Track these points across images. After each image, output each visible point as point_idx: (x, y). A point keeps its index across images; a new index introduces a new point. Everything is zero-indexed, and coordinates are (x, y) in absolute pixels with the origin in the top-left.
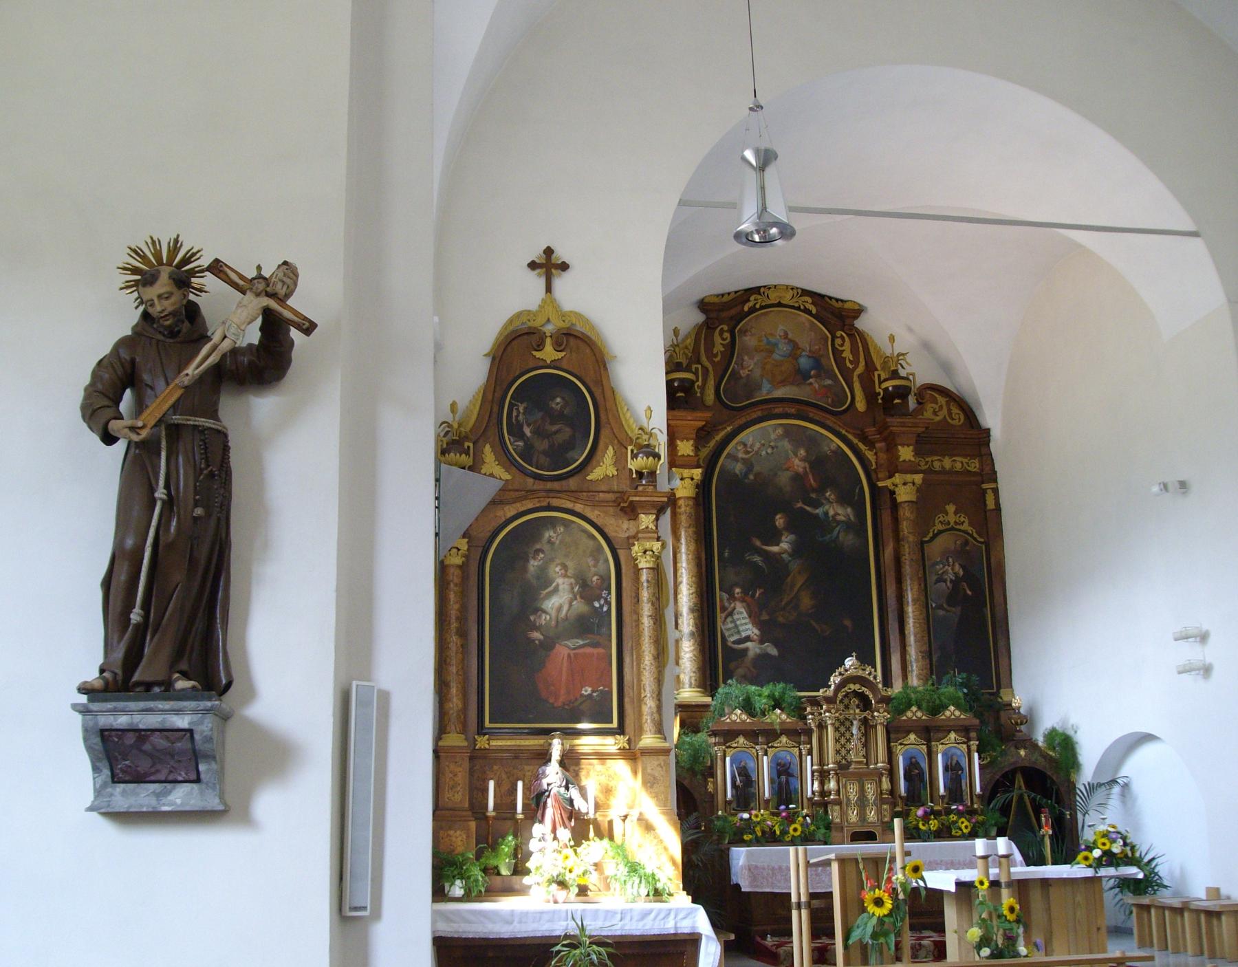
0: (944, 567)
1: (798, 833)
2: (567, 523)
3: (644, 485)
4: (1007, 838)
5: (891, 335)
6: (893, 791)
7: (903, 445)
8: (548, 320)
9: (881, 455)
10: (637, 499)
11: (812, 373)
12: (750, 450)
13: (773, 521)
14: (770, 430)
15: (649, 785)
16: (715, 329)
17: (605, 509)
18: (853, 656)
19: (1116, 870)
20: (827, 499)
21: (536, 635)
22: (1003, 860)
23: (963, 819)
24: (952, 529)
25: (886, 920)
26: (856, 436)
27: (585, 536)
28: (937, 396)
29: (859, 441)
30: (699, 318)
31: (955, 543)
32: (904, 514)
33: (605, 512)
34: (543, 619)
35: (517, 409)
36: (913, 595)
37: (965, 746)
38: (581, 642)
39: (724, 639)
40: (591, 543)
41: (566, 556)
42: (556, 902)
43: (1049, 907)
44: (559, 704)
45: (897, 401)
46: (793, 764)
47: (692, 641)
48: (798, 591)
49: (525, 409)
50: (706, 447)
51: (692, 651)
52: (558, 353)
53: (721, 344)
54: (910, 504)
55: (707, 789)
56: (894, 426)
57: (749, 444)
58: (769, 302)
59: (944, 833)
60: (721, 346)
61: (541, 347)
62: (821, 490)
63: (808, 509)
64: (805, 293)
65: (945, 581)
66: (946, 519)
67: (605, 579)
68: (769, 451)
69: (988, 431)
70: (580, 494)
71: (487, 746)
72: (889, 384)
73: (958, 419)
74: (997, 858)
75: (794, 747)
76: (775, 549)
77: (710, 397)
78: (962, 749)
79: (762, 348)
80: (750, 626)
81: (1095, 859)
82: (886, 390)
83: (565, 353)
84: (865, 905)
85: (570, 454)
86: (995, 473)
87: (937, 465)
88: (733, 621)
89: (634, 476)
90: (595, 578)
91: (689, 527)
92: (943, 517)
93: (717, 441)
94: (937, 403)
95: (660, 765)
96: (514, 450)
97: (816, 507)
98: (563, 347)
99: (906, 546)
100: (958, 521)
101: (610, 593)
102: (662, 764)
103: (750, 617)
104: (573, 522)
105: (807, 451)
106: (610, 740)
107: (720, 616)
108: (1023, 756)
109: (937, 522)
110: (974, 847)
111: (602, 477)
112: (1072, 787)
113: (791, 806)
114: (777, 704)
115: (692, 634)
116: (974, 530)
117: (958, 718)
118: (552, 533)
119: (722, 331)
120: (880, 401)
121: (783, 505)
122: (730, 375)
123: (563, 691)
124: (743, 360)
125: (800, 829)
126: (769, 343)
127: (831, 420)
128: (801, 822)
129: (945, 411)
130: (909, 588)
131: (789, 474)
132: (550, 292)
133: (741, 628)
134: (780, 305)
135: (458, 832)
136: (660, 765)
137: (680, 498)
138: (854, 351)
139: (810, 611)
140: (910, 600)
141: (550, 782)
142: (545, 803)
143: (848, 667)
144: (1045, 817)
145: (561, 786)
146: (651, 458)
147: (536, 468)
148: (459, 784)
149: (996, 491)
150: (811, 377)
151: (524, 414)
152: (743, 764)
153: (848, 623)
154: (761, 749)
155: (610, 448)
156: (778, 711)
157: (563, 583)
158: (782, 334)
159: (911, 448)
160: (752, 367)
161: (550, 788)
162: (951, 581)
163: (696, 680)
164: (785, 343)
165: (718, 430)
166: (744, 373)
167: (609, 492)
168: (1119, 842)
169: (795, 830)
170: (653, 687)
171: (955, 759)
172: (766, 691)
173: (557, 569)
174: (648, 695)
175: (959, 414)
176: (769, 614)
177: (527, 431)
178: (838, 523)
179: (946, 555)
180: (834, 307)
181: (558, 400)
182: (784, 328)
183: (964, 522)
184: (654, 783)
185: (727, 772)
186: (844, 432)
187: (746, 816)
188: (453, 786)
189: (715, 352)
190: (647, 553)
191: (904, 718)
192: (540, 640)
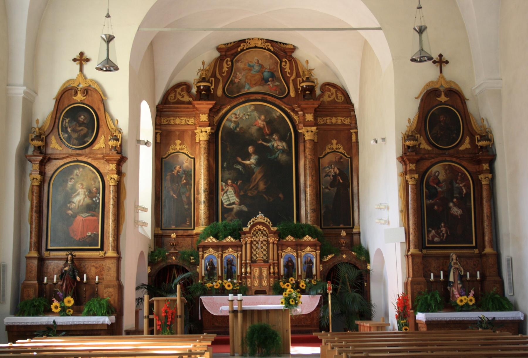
0: (329, 169)
2: (84, 167)
4: (241, 295)
6: (279, 272)
7: (308, 113)
12: (238, 117)
13: (248, 149)
14: (248, 107)
16: (224, 60)
20: (274, 139)
21: (70, 212)
26: (289, 109)
28: (331, 88)
29: (291, 111)
31: (336, 158)
32: (307, 146)
33: (100, 162)
34: (73, 206)
35: (66, 121)
37: (314, 253)
40: (93, 175)
41: (83, 180)
48: (258, 181)
49: (69, 121)
50: (217, 116)
53: (227, 67)
54: (310, 141)
57: (238, 114)
62: (271, 134)
63: (265, 143)
64: (268, 41)
65: (330, 176)
66: (332, 147)
67: (98, 189)
68: (247, 117)
72: (304, 85)
73: (341, 98)
76: (248, 162)
77: (220, 92)
79: (246, 68)
80: (235, 198)
85: (86, 139)
87: (328, 121)
88: (227, 196)
89: (479, 148)
90: (94, 189)
92: (330, 146)
94: (331, 92)
96: (64, 138)
97: (268, 143)
100: (337, 148)
101: (100, 195)
103: (235, 193)
104: (86, 167)
105: (265, 117)
107: (221, 193)
109: (327, 148)
115: (204, 202)
116: (345, 152)
117: (310, 241)
119: (227, 61)
120: (300, 92)
121: (252, 142)
122: (230, 82)
124: (236, 74)
125: (304, 285)
126: (250, 66)
127: (278, 102)
129: (334, 95)
131: (256, 127)
133: (230, 199)
134: (256, 47)
135: (31, 289)
136: (112, 263)
137: (201, 141)
138: (291, 68)
139: (263, 191)
146: (115, 141)
149: (356, 133)
151: (68, 123)
152: (211, 260)
153: (281, 196)
155: (103, 136)
158: (256, 61)
162: (333, 176)
163: (205, 222)
164: (257, 66)
166: (236, 81)
171: (309, 259)
173: (79, 186)
176: (243, 192)
177: (69, 130)
178: (279, 150)
179: (330, 164)
181: (82, 117)
186: (283, 107)
189: (223, 71)
192: (71, 214)
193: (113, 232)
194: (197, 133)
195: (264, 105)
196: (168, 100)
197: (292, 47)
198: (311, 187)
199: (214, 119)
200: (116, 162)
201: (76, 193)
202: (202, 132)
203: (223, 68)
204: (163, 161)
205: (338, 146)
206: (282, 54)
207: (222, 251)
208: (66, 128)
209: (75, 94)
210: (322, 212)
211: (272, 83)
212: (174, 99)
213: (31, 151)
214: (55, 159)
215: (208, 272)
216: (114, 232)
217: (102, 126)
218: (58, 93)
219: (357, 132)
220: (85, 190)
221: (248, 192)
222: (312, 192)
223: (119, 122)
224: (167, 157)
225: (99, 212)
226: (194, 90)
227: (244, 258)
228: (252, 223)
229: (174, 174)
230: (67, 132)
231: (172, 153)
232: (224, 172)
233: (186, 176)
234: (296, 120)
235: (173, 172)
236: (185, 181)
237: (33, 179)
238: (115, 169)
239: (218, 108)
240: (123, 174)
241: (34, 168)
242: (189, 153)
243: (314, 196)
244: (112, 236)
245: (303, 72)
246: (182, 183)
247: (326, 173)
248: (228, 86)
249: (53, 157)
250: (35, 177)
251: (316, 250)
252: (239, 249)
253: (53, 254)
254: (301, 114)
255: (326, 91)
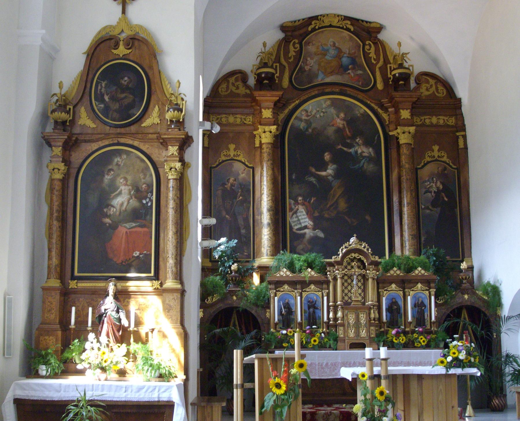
0: (430, 183)
1: (317, 343)
2: (128, 153)
3: (173, 128)
5: (399, 42)
6: (380, 318)
7: (403, 109)
8: (122, 31)
9: (392, 116)
10: (166, 136)
11: (350, 67)
12: (309, 114)
13: (323, 156)
14: (323, 102)
15: (167, 310)
17: (152, 144)
18: (354, 237)
19: (463, 370)
20: (357, 143)
21: (107, 221)
22: (383, 362)
23: (422, 337)
24: (436, 160)
25: (283, 397)
26: (377, 104)
27: (138, 161)
28: (429, 79)
30: (281, 35)
32: (403, 151)
33: (152, 146)
34: (112, 211)
35: (101, 85)
36: (407, 201)
37: (427, 292)
38: (134, 225)
39: (291, 227)
40: (142, 165)
41: (127, 173)
42: (100, 380)
43: (422, 392)
44: (120, 261)
45: (401, 82)
46: (318, 302)
47: (269, 229)
49: (106, 85)
51: (268, 235)
52: (127, 50)
53: (294, 51)
54: (407, 145)
55: (266, 316)
56: (397, 98)
57: (309, 111)
58: (324, 25)
59: (410, 345)
60: (294, 52)
61: (117, 47)
62: (353, 138)
63: (345, 149)
64: (346, 18)
65: (431, 192)
67: (150, 186)
69: (460, 100)
70: (137, 135)
71: (76, 287)
72: (396, 72)
73: (442, 92)
74: (380, 360)
75: (319, 291)
76: (323, 173)
77: (286, 83)
78: (425, 293)
80: (307, 220)
81: (448, 362)
82: (394, 75)
83: (131, 50)
84: (271, 387)
85: (131, 112)
86: (464, 125)
87: (427, 121)
88: (297, 217)
90: (144, 186)
91: (268, 161)
92: (431, 153)
93: (289, 109)
95: (174, 298)
96: (98, 110)
97: (350, 148)
98: (130, 46)
99: (404, 170)
100: (440, 155)
101: (152, 195)
102: (175, 298)
103: (307, 214)
105: (345, 115)
106: (148, 283)
107: (289, 214)
108: (466, 299)
109: (426, 156)
110: (364, 354)
111: (151, 124)
112: (498, 318)
113: (314, 327)
114: (310, 265)
115: (269, 224)
116: (450, 161)
117: (423, 275)
118: (119, 159)
119: (294, 44)
120: (391, 83)
121: (329, 147)
123: (122, 254)
124: (307, 60)
125: (318, 341)
127: (361, 96)
128: (318, 336)
130: (405, 196)
131: (333, 128)
132: (125, 14)
133: (302, 221)
134: (331, 26)
136: (174, 298)
137: (263, 144)
140: (405, 203)
141: (106, 308)
142: (103, 321)
143: (351, 243)
144: (465, 336)
145: (113, 311)
146: (176, 112)
147: (111, 120)
148: (53, 309)
149: (465, 137)
150: (349, 70)
151: (105, 87)
152: (287, 301)
153: (368, 218)
154: (298, 292)
155: (157, 107)
156: (309, 270)
157: (125, 189)
158: (332, 44)
159: (409, 111)
160: (312, 64)
161: (106, 311)
162: (435, 192)
163: (270, 252)
165: (291, 103)
166: (307, 68)
167: (155, 134)
168: (463, 352)
169: (315, 341)
170: (173, 251)
172: (303, 258)
174: (170, 256)
175: (443, 90)
177: (106, 98)
179: (431, 177)
180: (364, 26)
181: (126, 78)
182: (333, 40)
183: (444, 156)
184: (170, 310)
185: (276, 304)
186: (369, 102)
187: (284, 332)
188: (50, 310)
189: (290, 56)
190: (172, 170)
191: (389, 274)
192: (109, 224)
193: (175, 250)
194: (257, 135)
195: (344, 100)
196: (218, 91)
197: (378, 26)
198: (410, 205)
199: (279, 117)
200: (178, 144)
201: (117, 192)
202: (264, 132)
203: (289, 52)
204: (212, 171)
205: (441, 153)
206: (364, 34)
207: (302, 289)
208: (103, 95)
209: (115, 46)
210: (423, 239)
211: (354, 71)
212: (226, 91)
213: (49, 128)
214: (86, 141)
215: (283, 318)
216: (177, 250)
217: (156, 91)
218: (90, 45)
219: (466, 135)
220: (130, 187)
221: (324, 212)
222: (412, 212)
223: (181, 85)
224: (217, 166)
225: (152, 221)
226: (252, 81)
227: (331, 299)
228: (344, 251)
229: (227, 188)
230: (102, 101)
231: (223, 161)
232: (292, 186)
233: (242, 191)
234: (385, 120)
235: (226, 186)
236: (241, 198)
237: (53, 170)
238: (177, 154)
239: (284, 103)
240: (188, 164)
241: (54, 153)
242: (246, 160)
243: (414, 218)
244: (173, 256)
245: (394, 58)
246: (238, 200)
247: (426, 188)
248: (296, 75)
249: (81, 138)
250: (56, 166)
251: (430, 288)
252: (325, 286)
253: (83, 285)
254: (392, 112)
255: (423, 82)
